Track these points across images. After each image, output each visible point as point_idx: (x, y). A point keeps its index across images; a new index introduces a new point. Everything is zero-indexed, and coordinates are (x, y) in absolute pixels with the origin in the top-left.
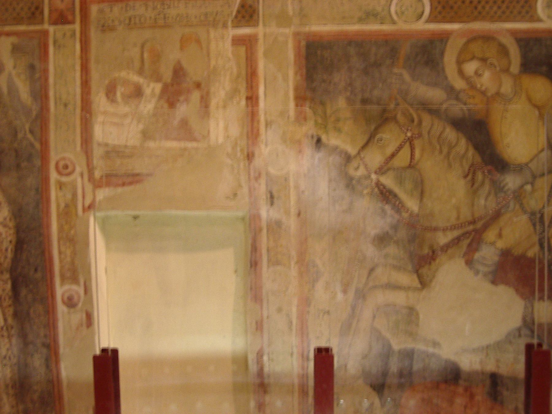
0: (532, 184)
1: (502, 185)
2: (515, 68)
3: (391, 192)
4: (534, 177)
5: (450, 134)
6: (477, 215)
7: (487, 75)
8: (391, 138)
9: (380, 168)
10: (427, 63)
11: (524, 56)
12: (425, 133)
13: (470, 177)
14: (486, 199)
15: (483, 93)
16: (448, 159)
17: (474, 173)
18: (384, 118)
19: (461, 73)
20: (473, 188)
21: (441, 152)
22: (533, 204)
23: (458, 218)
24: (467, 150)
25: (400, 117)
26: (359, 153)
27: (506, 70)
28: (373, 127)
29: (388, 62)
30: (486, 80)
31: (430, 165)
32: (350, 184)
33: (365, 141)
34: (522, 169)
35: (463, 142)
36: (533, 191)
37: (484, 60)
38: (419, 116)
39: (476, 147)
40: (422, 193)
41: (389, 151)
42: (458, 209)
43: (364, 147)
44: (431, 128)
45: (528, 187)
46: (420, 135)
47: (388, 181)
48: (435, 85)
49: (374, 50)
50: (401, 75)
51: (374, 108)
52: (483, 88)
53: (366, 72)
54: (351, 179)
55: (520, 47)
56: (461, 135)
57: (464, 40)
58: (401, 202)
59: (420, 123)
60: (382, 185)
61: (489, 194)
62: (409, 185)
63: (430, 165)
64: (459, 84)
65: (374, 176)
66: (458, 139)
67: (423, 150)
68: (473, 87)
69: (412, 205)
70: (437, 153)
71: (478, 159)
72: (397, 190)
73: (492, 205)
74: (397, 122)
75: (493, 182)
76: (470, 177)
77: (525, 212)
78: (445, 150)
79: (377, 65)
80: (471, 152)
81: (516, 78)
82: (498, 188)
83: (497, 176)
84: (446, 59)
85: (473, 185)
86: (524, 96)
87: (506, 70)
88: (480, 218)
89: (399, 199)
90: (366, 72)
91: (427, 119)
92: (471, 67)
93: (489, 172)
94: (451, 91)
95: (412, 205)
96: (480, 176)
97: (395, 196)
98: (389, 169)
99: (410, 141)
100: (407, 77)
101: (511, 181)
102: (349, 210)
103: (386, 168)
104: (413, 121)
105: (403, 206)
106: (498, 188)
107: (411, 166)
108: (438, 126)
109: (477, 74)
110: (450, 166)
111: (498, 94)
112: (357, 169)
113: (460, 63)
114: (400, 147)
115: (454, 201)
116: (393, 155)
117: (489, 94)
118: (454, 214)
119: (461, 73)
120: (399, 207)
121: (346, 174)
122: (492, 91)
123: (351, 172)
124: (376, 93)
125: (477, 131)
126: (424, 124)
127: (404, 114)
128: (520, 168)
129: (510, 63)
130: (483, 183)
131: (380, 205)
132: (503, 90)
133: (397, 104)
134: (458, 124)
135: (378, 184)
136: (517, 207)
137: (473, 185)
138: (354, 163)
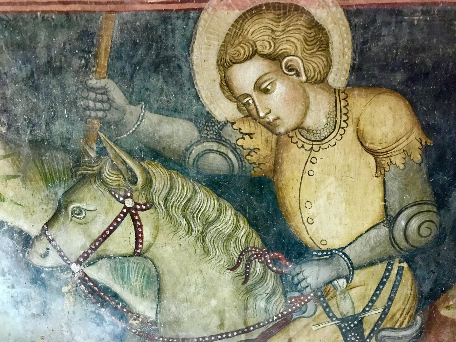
0: (348, 279)
1: (296, 280)
2: (338, 77)
3: (106, 290)
4: (353, 268)
5: (206, 201)
6: (251, 322)
7: (280, 90)
8: (98, 207)
9: (86, 256)
10: (156, 67)
11: (360, 51)
12: (158, 200)
13: (240, 269)
14: (268, 301)
15: (270, 127)
16: (204, 241)
17: (249, 262)
18: (80, 174)
19: (226, 85)
20: (247, 284)
21: (190, 231)
22: (345, 306)
23: (222, 325)
24: (237, 227)
25: (107, 173)
26: (43, 232)
27: (322, 81)
28: (60, 192)
29: (77, 63)
30: (279, 102)
31: (170, 248)
32: (37, 277)
33: (50, 214)
34: (332, 255)
35: (229, 214)
36: (348, 289)
37: (274, 58)
38: (144, 170)
39: (253, 223)
40: (160, 291)
41: (97, 229)
42: (221, 314)
43: (49, 224)
44: (168, 194)
45: (342, 282)
46: (149, 205)
47: (100, 274)
48: (175, 112)
49: (42, 36)
50: (105, 91)
51: (60, 160)
52: (271, 118)
53: (32, 83)
54: (38, 271)
55: (353, 27)
56: (224, 203)
57: (236, 13)
58: (125, 305)
59: (149, 182)
60: (90, 280)
61: (274, 293)
62: (137, 281)
63: (170, 248)
64: (223, 109)
65: (75, 268)
66: (220, 211)
67: (157, 228)
68: (250, 115)
69: (144, 307)
70: (182, 233)
71: (256, 241)
72: (117, 288)
73: (278, 306)
74: (104, 183)
75: (281, 276)
76: (240, 269)
77: (332, 317)
78: (198, 227)
79: (54, 69)
80: (244, 229)
81: (339, 96)
82: (288, 284)
83: (289, 268)
84: (196, 57)
85: (245, 282)
86: (350, 131)
87: (322, 81)
88: (258, 326)
89: (122, 301)
90: (32, 83)
91: (160, 175)
92: (246, 75)
93: (275, 261)
94: (206, 122)
95: (144, 307)
96: (258, 267)
97: (116, 296)
98: (100, 258)
99: (133, 213)
100: (117, 95)
101: (313, 274)
102: (44, 312)
103: (94, 256)
104: (135, 182)
105: (129, 311)
106: (288, 284)
107: (138, 252)
108: (183, 187)
109: (262, 89)
110: (207, 252)
111: (299, 128)
112: (45, 256)
113: (224, 64)
114: (116, 223)
115: (214, 302)
116: (105, 236)
117: (282, 130)
118: (215, 321)
119: (226, 85)
120: (123, 311)
121: (28, 264)
122: (288, 121)
123: (37, 261)
124: (58, 127)
125: (257, 197)
126: (157, 185)
127: (115, 167)
128: (329, 255)
129: (329, 65)
130: (263, 278)
131: (91, 307)
132: (309, 122)
133: (102, 152)
134: (218, 185)
135: (85, 279)
136: (320, 309)
137: (245, 282)
138: (40, 247)
